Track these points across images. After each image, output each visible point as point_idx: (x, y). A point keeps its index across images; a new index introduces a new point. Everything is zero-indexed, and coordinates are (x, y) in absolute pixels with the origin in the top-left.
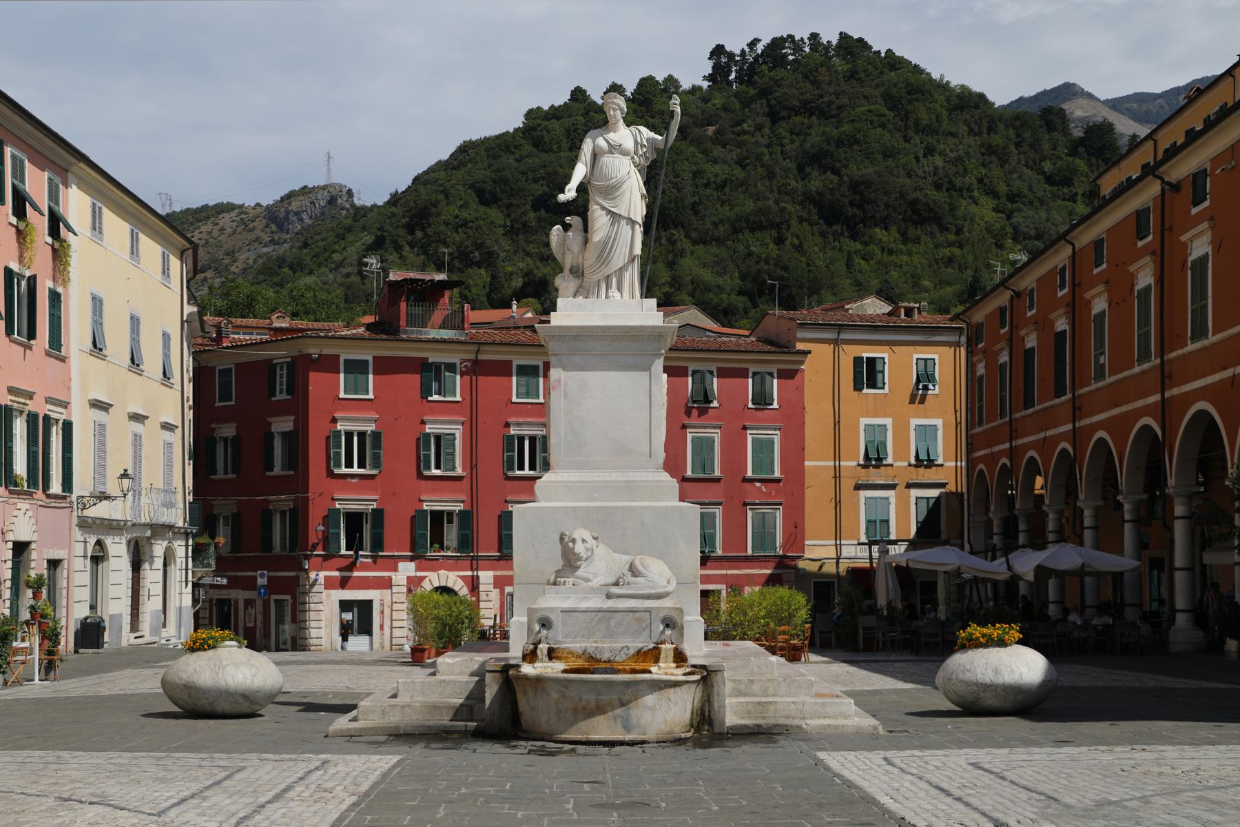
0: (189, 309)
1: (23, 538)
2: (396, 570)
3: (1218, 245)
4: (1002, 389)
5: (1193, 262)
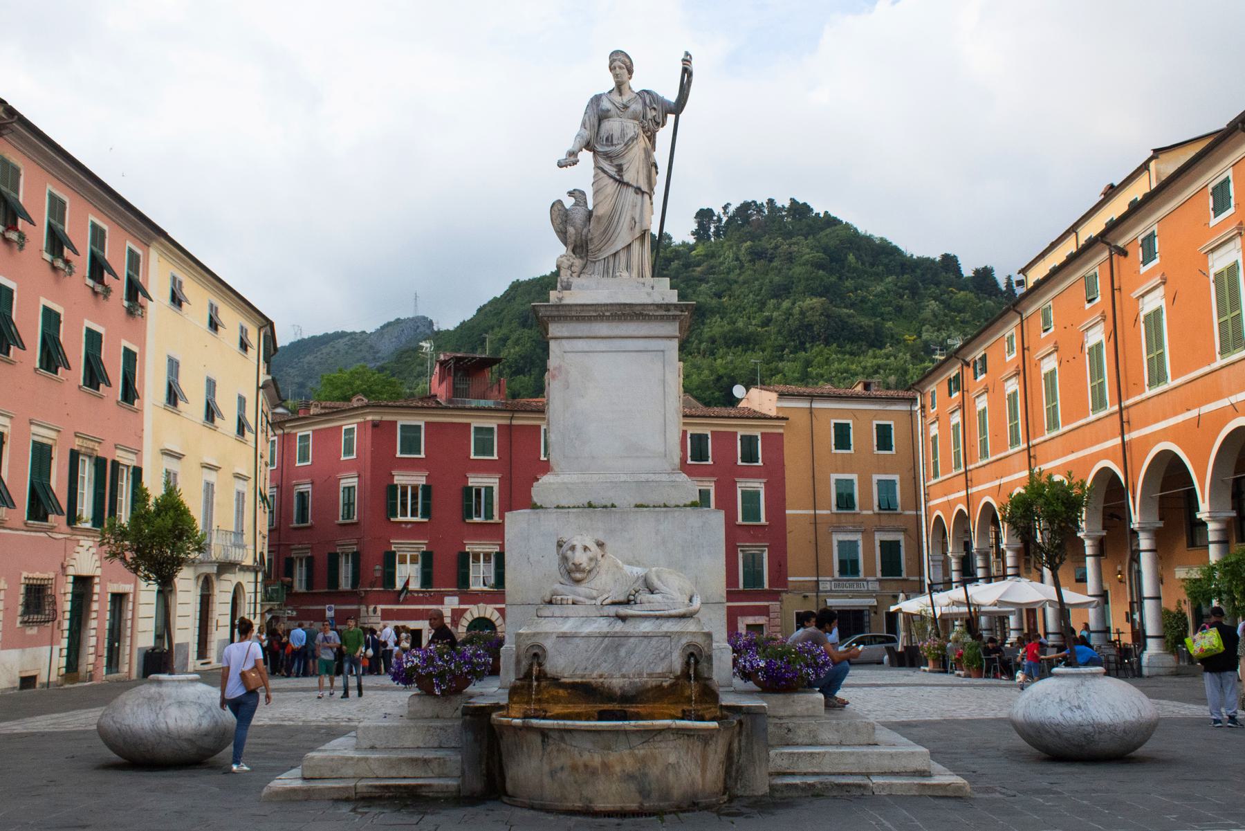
0: (264, 377)
1: (85, 572)
2: (442, 603)
3: (1173, 299)
4: (1014, 416)
5: (1147, 317)
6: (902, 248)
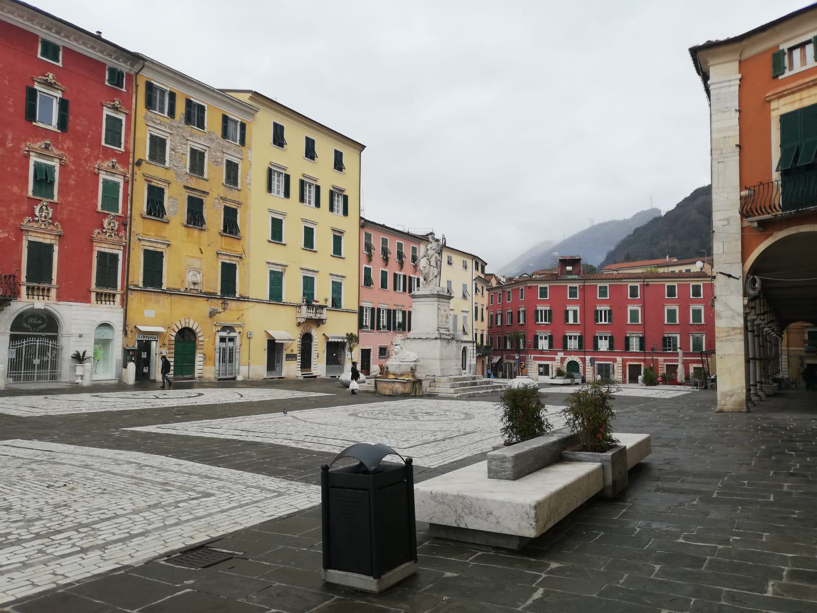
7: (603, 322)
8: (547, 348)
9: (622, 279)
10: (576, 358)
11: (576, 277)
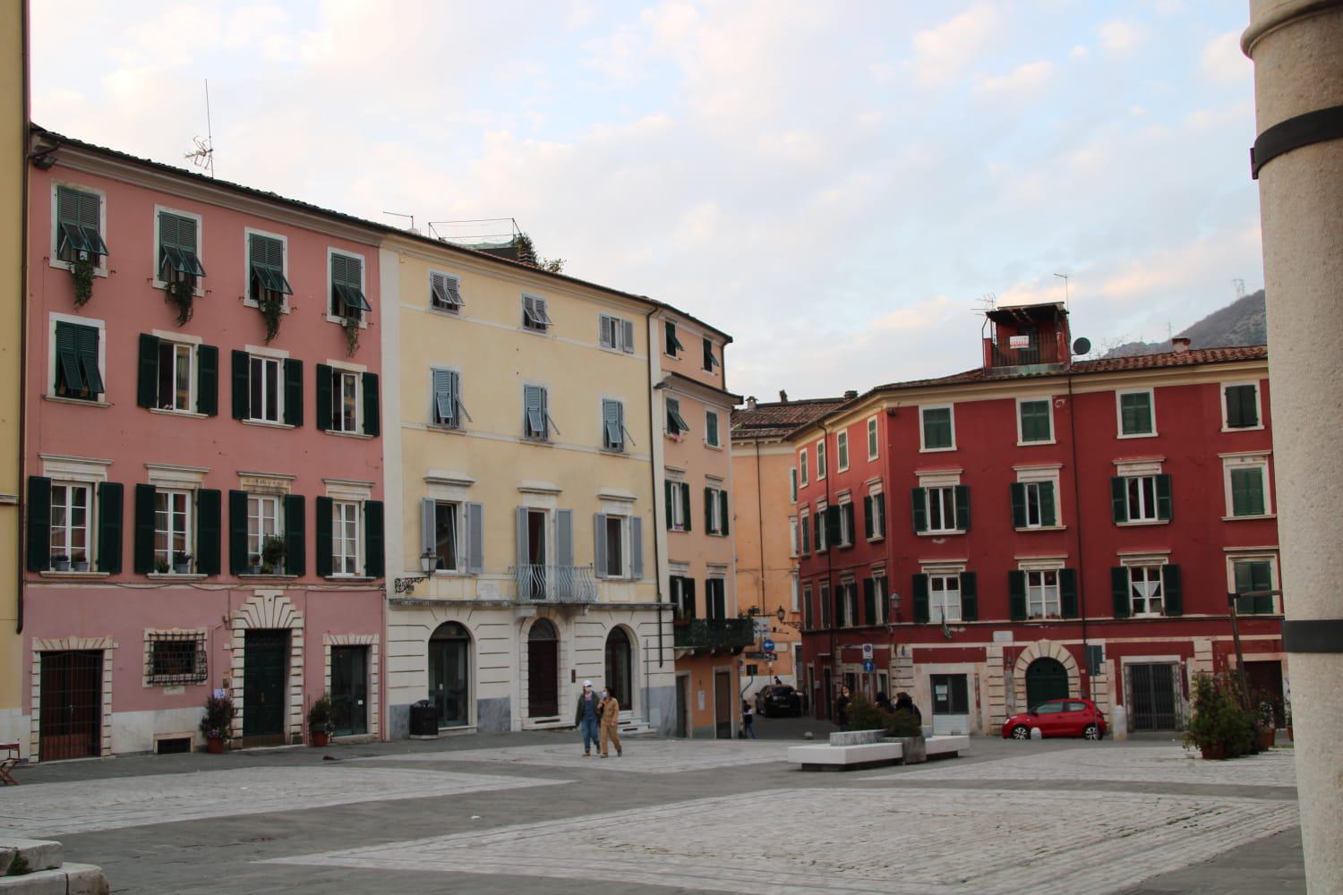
2: (991, 639)
6: (251, 187)
7: (1143, 520)
8: (958, 620)
9: (1196, 364)
10: (1056, 649)
11: (1043, 368)
